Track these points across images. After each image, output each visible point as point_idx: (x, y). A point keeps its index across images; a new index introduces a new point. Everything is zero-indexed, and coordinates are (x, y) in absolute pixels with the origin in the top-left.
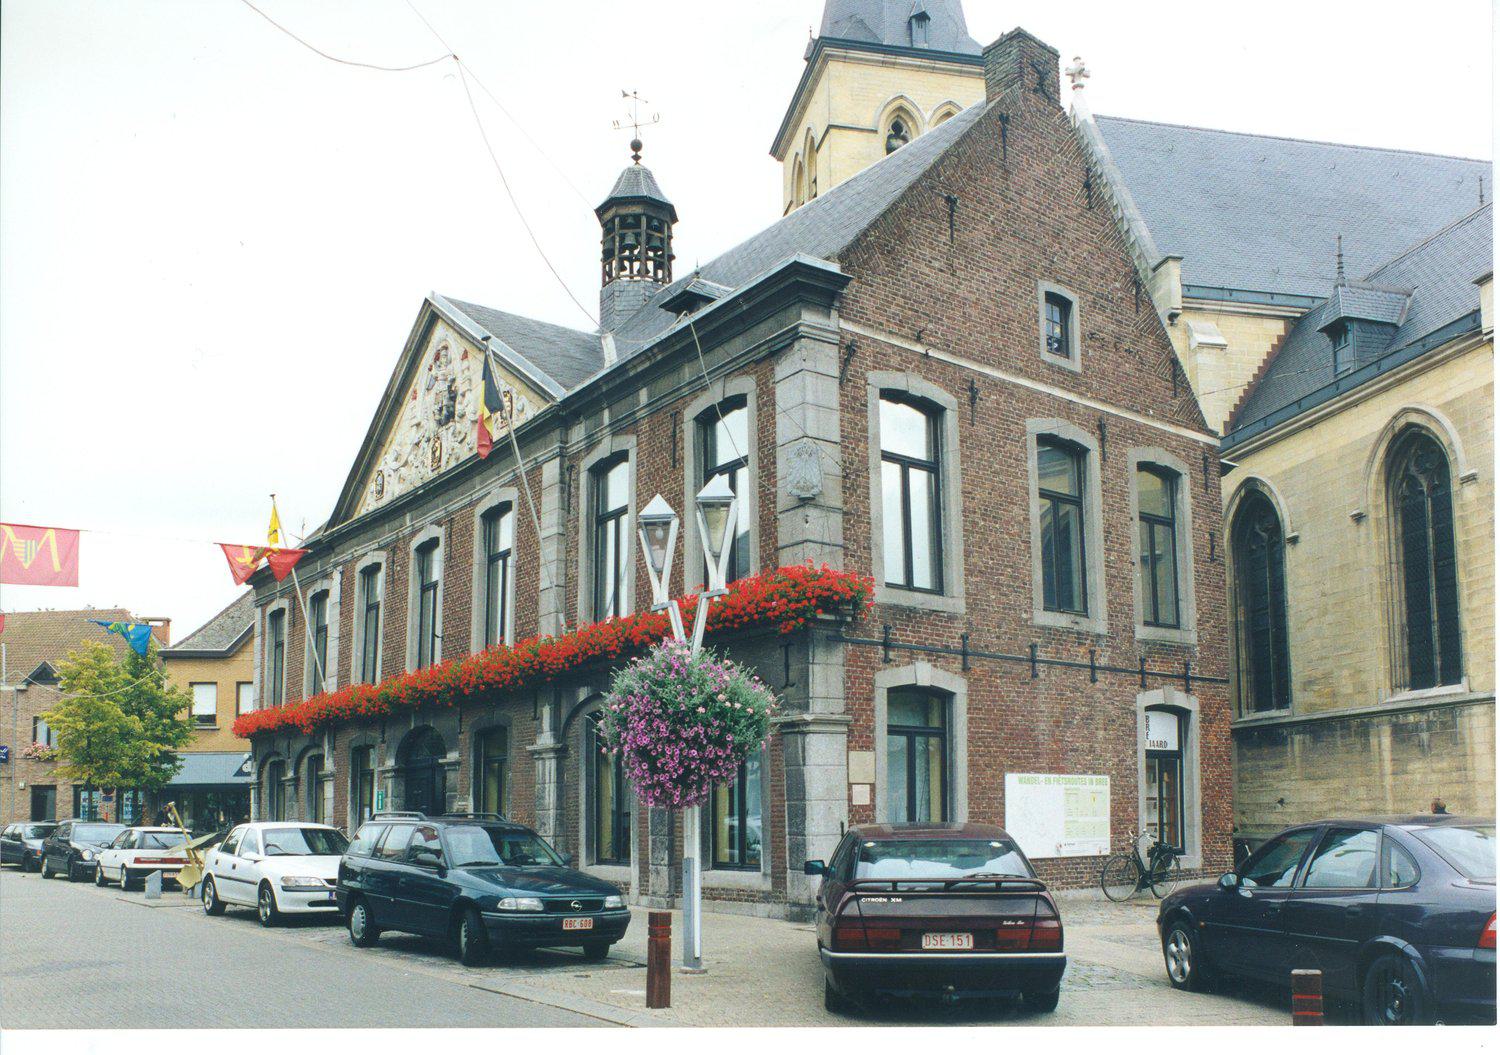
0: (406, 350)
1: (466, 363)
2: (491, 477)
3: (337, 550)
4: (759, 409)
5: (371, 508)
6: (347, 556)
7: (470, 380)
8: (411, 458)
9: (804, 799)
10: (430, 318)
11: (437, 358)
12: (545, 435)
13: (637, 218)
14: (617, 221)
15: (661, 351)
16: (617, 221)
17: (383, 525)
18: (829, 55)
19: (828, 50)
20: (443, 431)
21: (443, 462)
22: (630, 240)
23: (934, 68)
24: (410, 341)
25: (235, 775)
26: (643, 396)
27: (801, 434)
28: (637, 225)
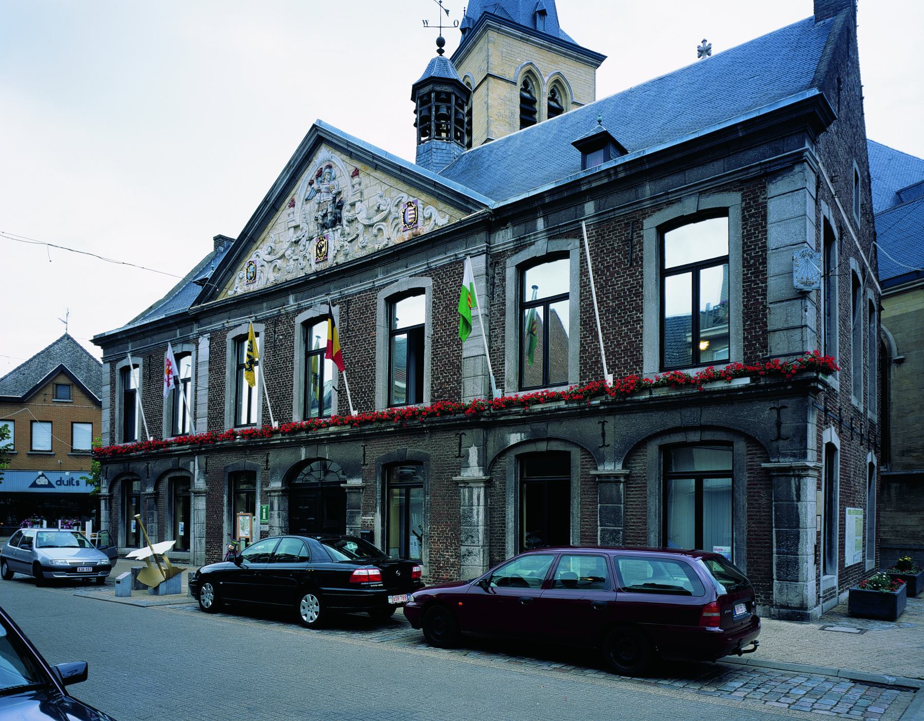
0: (289, 166)
1: (356, 179)
2: (398, 268)
3: (202, 322)
4: (744, 219)
5: (240, 291)
6: (217, 326)
7: (362, 193)
8: (289, 252)
9: (798, 526)
10: (319, 137)
11: (320, 174)
12: (467, 236)
13: (448, 95)
14: (433, 95)
15: (625, 170)
16: (433, 95)
17: (262, 303)
18: (488, 26)
19: (489, 22)
20: (329, 232)
21: (330, 256)
22: (443, 111)
23: (550, 48)
24: (294, 158)
25: (31, 486)
26: (590, 208)
27: (800, 240)
28: (449, 101)
